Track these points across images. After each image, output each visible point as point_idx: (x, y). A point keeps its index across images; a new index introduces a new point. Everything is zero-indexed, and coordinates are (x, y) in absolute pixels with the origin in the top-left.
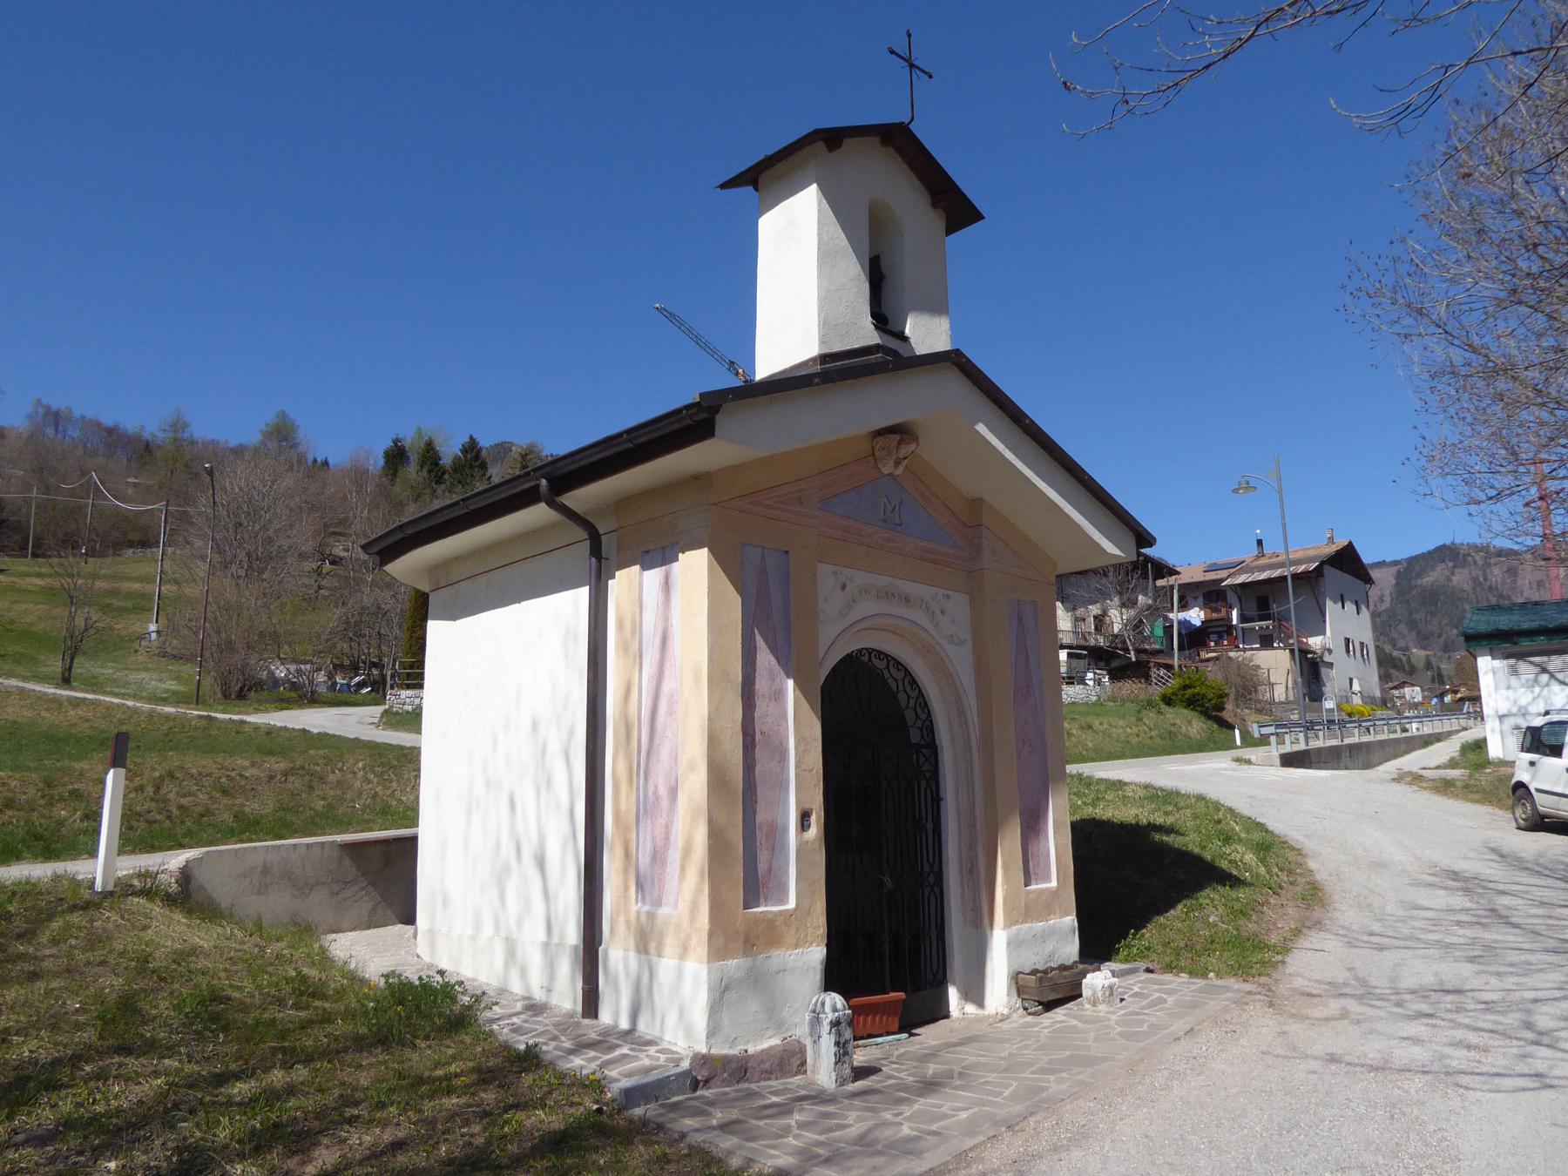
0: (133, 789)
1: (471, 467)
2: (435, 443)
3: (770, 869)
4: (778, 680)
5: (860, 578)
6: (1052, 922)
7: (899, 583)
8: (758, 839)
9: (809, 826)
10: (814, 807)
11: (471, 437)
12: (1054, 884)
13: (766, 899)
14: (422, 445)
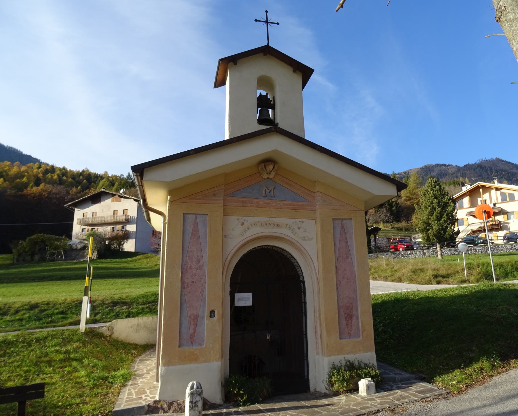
9: (214, 316)
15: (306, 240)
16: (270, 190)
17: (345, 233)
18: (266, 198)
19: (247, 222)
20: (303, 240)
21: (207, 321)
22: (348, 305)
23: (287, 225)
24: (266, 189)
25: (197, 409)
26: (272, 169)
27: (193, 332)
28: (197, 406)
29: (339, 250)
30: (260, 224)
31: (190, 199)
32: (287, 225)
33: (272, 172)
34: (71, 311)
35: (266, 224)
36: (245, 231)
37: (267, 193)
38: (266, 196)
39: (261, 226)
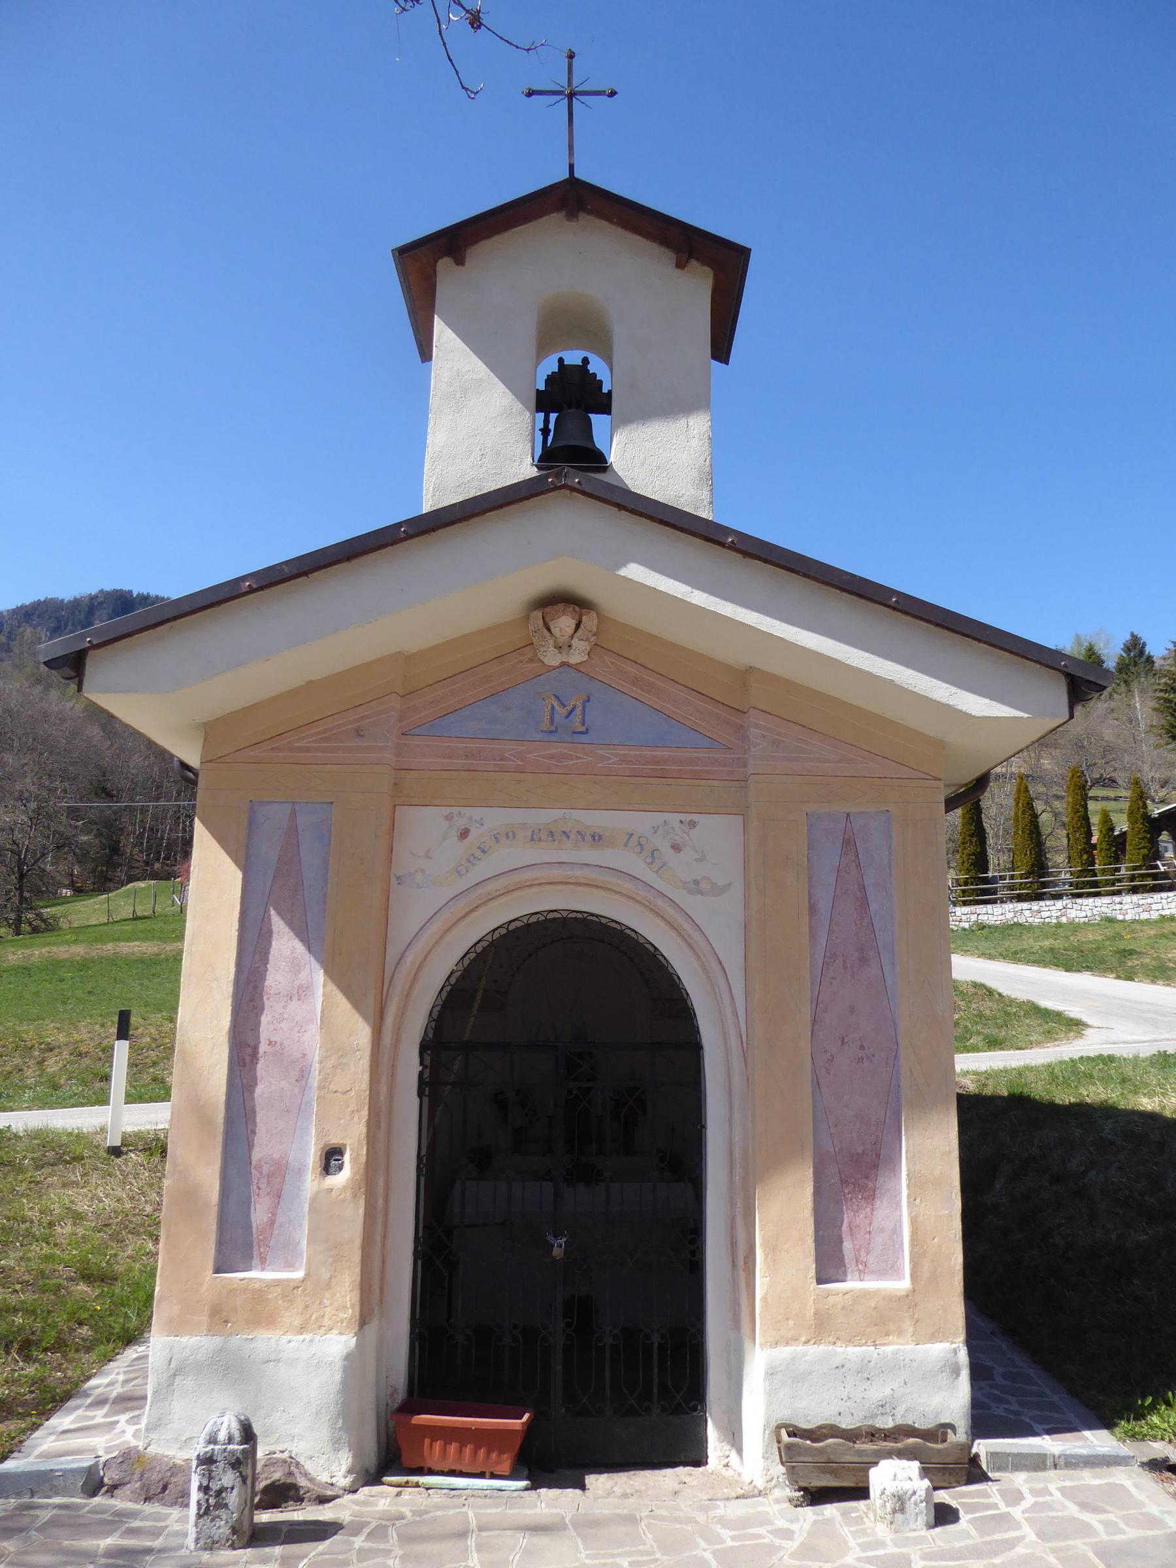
0: (135, 1050)
1: (1136, 664)
2: (1096, 648)
4: (304, 974)
5: (497, 818)
6: (889, 1349)
7: (577, 814)
9: (340, 1168)
10: (348, 1142)
11: (1132, 635)
12: (904, 1284)
13: (263, 1261)
14: (1083, 652)
15: (702, 894)
16: (569, 708)
17: (859, 866)
18: (553, 738)
19: (482, 825)
20: (691, 892)
21: (311, 1182)
22: (860, 1150)
24: (555, 704)
25: (222, 1513)
26: (571, 631)
27: (266, 1219)
28: (226, 1506)
29: (830, 931)
31: (273, 749)
33: (575, 642)
35: (551, 834)
36: (472, 860)
37: (557, 719)
38: (553, 728)
39: (532, 840)
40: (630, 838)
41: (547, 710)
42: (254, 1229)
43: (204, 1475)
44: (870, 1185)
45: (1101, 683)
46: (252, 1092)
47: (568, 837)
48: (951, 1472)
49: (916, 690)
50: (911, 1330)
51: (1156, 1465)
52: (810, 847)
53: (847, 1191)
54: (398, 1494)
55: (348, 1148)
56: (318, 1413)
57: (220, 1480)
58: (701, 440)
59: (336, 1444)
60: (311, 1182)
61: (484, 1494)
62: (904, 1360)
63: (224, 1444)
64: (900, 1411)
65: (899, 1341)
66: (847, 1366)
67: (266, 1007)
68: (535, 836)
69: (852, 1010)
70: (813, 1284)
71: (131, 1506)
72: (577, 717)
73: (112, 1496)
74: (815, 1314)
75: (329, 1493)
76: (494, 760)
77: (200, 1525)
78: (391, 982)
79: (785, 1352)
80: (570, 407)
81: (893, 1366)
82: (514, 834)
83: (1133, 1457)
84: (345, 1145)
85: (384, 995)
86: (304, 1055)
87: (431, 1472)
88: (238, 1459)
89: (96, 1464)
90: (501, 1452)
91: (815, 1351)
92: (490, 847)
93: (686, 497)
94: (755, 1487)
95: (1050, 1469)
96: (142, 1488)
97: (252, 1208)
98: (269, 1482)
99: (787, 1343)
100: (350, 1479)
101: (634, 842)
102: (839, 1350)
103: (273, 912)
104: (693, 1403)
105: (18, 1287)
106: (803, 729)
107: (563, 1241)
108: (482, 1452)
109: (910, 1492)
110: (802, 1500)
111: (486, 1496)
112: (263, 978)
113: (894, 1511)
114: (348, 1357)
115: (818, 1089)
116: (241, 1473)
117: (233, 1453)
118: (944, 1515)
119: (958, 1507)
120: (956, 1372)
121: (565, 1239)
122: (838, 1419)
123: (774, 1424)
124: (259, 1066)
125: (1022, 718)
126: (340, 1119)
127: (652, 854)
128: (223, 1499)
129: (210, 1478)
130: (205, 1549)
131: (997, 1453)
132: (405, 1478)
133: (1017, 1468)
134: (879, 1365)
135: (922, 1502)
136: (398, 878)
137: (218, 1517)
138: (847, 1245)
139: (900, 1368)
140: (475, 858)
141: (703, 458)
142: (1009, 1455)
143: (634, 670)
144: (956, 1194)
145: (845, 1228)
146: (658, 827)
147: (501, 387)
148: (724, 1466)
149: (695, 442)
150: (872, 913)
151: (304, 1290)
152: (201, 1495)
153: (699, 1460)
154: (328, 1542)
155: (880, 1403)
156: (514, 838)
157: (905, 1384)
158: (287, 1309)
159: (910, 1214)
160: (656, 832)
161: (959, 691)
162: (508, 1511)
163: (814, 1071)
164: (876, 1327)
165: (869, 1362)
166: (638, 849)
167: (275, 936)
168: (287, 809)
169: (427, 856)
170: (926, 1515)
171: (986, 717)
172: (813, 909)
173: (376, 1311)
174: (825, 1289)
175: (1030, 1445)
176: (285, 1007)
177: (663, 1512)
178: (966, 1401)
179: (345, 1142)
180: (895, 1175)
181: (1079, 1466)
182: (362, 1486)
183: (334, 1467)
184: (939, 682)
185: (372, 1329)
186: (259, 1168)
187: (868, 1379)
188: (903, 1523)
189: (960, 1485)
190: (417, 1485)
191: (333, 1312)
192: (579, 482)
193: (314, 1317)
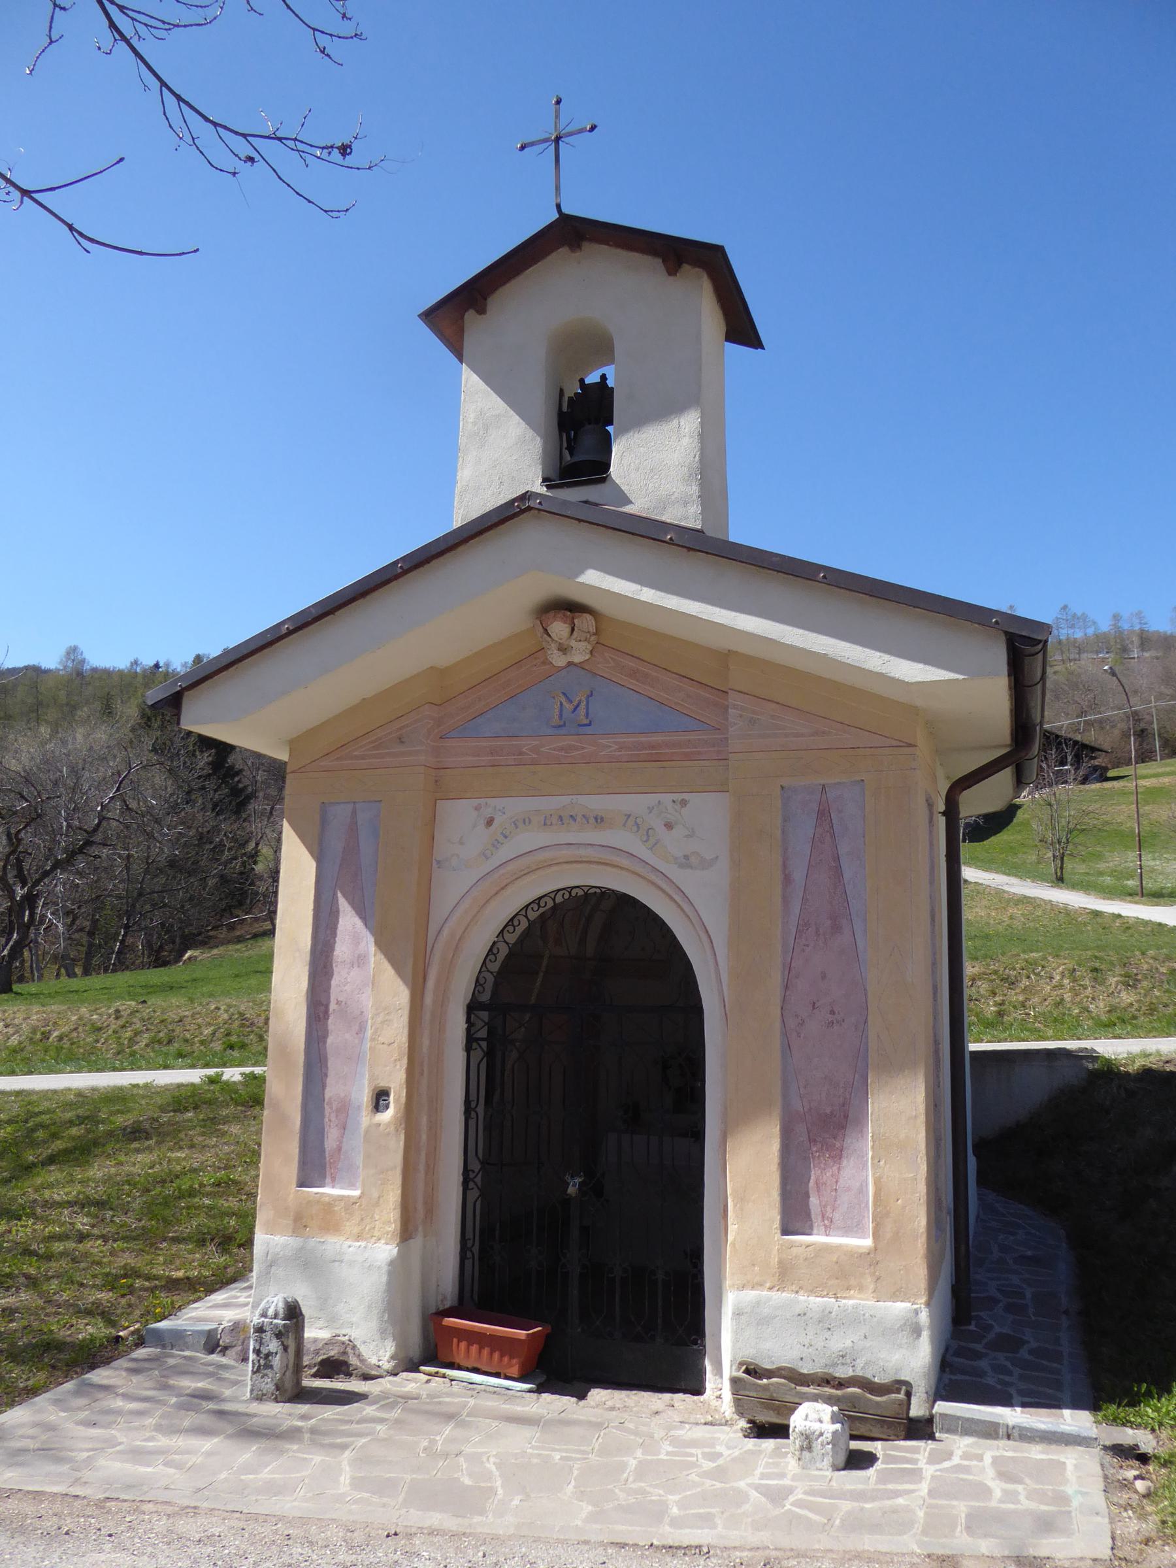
3: (339, 1149)
4: (363, 944)
7: (583, 800)
8: (327, 1115)
9: (387, 1107)
10: (392, 1086)
13: (333, 1179)
15: (691, 867)
16: (575, 703)
17: (833, 835)
20: (681, 866)
22: (828, 1111)
23: (629, 816)
24: (563, 700)
25: (268, 1371)
27: (335, 1146)
28: (271, 1367)
29: (804, 900)
30: (542, 818)
31: (337, 759)
32: (629, 816)
34: (974, 1024)
36: (496, 844)
37: (564, 716)
38: (562, 723)
39: (545, 824)
40: (627, 819)
41: (557, 706)
42: (327, 1153)
43: (256, 1340)
44: (838, 1145)
45: (1035, 637)
46: (325, 1043)
47: (575, 820)
48: (890, 1425)
49: (848, 661)
50: (872, 1287)
51: (1122, 1451)
52: (786, 819)
53: (815, 1149)
54: (428, 1381)
55: (392, 1090)
56: (370, 1307)
57: (268, 1346)
58: (692, 437)
59: (383, 1333)
60: (365, 1118)
61: (495, 1392)
62: (864, 1315)
63: (271, 1318)
64: (860, 1363)
65: (859, 1296)
66: (809, 1315)
67: (335, 973)
68: (547, 821)
69: (824, 976)
70: (778, 1235)
71: (232, 1363)
72: (582, 711)
73: (224, 1355)
74: (780, 1262)
75: (374, 1373)
76: (514, 755)
77: (254, 1379)
78: (431, 953)
79: (751, 1295)
80: (590, 424)
81: (853, 1320)
82: (530, 820)
83: (1096, 1439)
84: (390, 1088)
85: (427, 961)
86: (362, 1012)
87: (460, 1368)
88: (280, 1331)
89: (216, 1329)
90: (512, 1357)
91: (778, 1297)
92: (511, 833)
93: (676, 494)
94: (725, 1417)
95: (1002, 1438)
96: (242, 1351)
97: (326, 1136)
98: (325, 1357)
99: (753, 1288)
100: (392, 1363)
101: (630, 821)
102: (802, 1298)
103: (339, 895)
104: (694, 1337)
105: (244, 1197)
106: (778, 706)
107: (578, 1180)
108: (496, 1355)
109: (817, 1433)
110: (749, 1431)
111: (495, 1392)
112: (332, 949)
113: (802, 1449)
114: (392, 1263)
115: (788, 1051)
116: (282, 1343)
117: (276, 1326)
118: (858, 1461)
119: (881, 1457)
120: (917, 1331)
121: (580, 1180)
122: (800, 1363)
123: (739, 1360)
124: (330, 1021)
125: (957, 679)
126: (386, 1066)
127: (647, 832)
128: (270, 1361)
129: (261, 1344)
130: (257, 1399)
131: (946, 1415)
132: (436, 1370)
133: (966, 1432)
134: (839, 1317)
135: (828, 1444)
136: (438, 862)
137: (267, 1375)
138: (814, 1201)
139: (860, 1322)
140: (498, 842)
141: (692, 454)
142: (959, 1418)
143: (631, 664)
144: (921, 1158)
145: (812, 1184)
146: (653, 807)
147: (516, 418)
148: (717, 1397)
149: (686, 441)
150: (845, 882)
151: (360, 1206)
152: (255, 1356)
153: (698, 1390)
154: (346, 1407)
155: (841, 1353)
156: (530, 823)
157: (865, 1337)
158: (348, 1220)
159: (873, 1174)
160: (650, 812)
161: (892, 658)
162: (503, 1406)
163: (785, 1033)
164: (836, 1281)
165: (830, 1313)
166: (635, 828)
167: (341, 915)
168: (350, 807)
169: (461, 843)
170: (832, 1456)
171: (920, 682)
172: (787, 880)
173: (420, 1229)
174: (788, 1240)
175: (991, 1414)
176: (348, 973)
177: (632, 1426)
178: (927, 1361)
179: (390, 1086)
180: (862, 1137)
181: (1035, 1441)
182: (403, 1372)
183: (381, 1353)
184: (873, 652)
185: (417, 1243)
186: (330, 1104)
187: (829, 1329)
188: (810, 1461)
189: (899, 1440)
190: (444, 1376)
191: (381, 1225)
192: (540, 503)
193: (367, 1228)
